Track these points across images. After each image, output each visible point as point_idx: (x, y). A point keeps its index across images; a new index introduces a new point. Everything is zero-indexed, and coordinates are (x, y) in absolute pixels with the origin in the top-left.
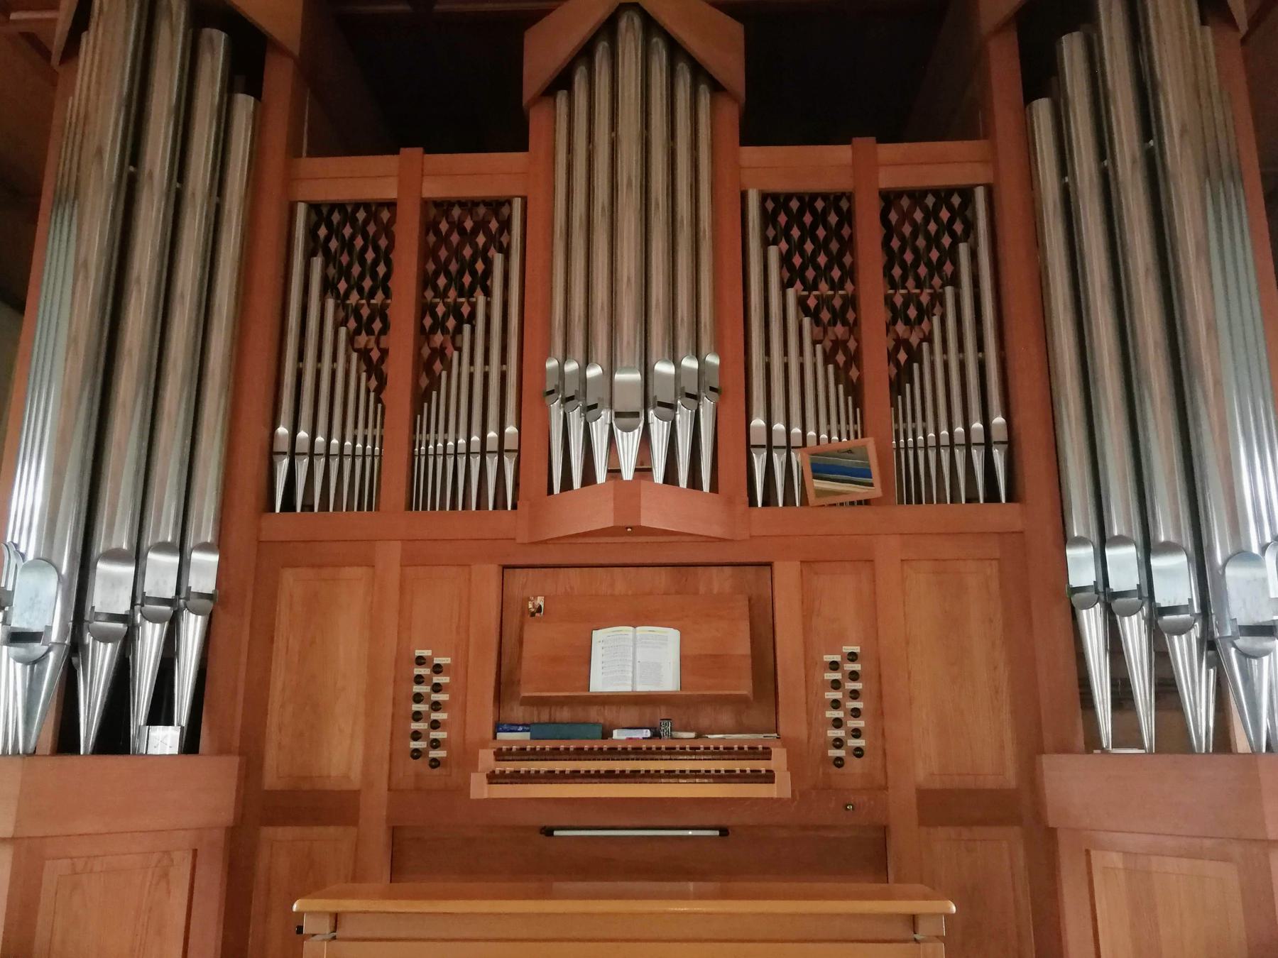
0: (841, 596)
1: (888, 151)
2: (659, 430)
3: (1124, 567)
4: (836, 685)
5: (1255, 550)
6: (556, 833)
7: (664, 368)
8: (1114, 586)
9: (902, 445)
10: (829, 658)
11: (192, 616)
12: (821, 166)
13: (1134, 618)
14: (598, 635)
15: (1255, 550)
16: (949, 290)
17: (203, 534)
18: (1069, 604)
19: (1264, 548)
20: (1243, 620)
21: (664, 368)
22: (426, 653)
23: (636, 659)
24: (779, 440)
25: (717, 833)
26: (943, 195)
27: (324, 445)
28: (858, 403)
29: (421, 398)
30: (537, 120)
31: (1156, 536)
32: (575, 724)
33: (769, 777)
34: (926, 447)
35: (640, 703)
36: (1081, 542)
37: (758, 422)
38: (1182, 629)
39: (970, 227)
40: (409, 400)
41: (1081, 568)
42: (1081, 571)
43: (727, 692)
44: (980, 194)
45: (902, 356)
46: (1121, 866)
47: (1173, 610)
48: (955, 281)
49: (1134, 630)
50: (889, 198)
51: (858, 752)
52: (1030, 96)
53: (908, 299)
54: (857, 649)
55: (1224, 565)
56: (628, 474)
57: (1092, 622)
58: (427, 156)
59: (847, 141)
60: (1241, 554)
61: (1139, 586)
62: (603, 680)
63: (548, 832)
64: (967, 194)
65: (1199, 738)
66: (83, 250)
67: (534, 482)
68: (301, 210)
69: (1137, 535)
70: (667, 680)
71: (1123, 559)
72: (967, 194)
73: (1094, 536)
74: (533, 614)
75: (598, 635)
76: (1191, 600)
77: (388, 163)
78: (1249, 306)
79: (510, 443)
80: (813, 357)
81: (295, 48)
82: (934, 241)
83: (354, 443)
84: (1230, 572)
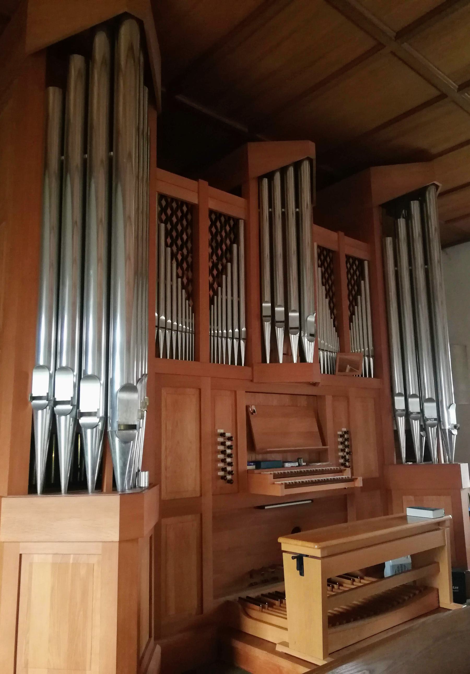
1: (348, 240)
3: (65, 387)
6: (266, 508)
9: (212, 334)
12: (186, 189)
16: (229, 264)
25: (310, 501)
34: (214, 336)
43: (312, 448)
46: (413, 500)
47: (89, 414)
48: (231, 261)
52: (385, 234)
57: (401, 421)
58: (158, 169)
59: (196, 179)
63: (262, 507)
64: (236, 221)
65: (434, 459)
66: (127, 209)
74: (252, 414)
83: (214, 331)
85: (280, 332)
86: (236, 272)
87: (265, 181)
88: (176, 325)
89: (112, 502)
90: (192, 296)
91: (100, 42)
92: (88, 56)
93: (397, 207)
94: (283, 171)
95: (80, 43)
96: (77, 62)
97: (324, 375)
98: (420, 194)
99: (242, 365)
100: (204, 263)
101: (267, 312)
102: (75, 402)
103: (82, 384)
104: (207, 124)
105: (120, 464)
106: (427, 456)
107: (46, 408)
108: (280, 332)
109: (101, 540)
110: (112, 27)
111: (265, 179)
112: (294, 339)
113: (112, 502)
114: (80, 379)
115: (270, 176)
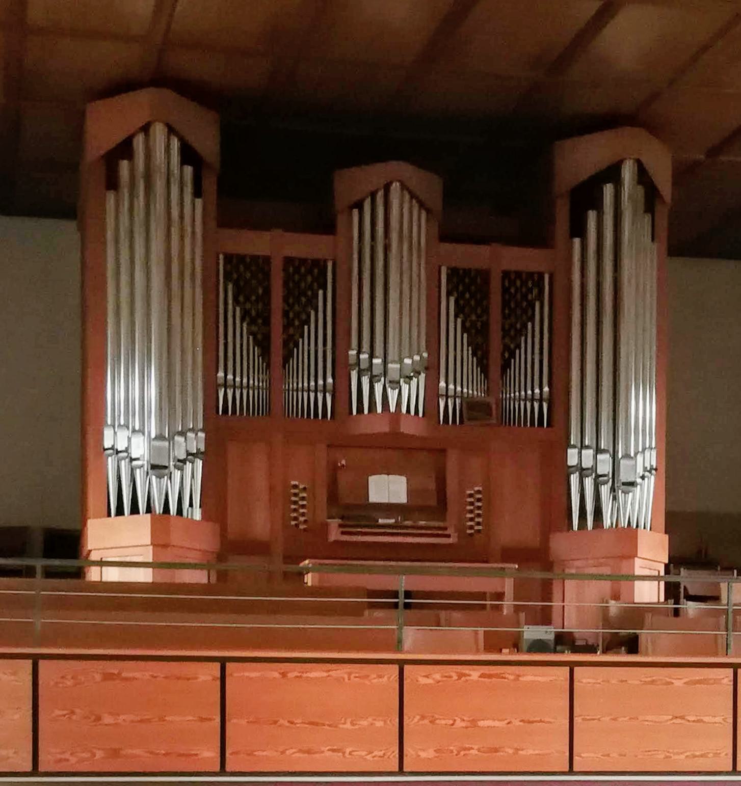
0: (476, 464)
2: (405, 388)
4: (472, 504)
5: (632, 455)
7: (408, 361)
8: (584, 466)
10: (469, 492)
11: (199, 460)
13: (590, 478)
15: (632, 455)
17: (199, 425)
18: (567, 471)
19: (636, 454)
20: (624, 480)
22: (296, 483)
23: (388, 488)
24: (451, 393)
27: (239, 382)
28: (486, 377)
29: (286, 360)
31: (330, 537)
33: (449, 536)
35: (389, 509)
36: (574, 447)
37: (442, 384)
38: (606, 483)
39: (541, 292)
41: (572, 457)
42: (572, 460)
44: (547, 277)
45: (507, 355)
48: (532, 319)
49: (589, 482)
51: (479, 531)
54: (481, 489)
55: (621, 458)
56: (392, 409)
57: (574, 479)
60: (627, 456)
61: (592, 466)
62: (374, 498)
67: (342, 409)
68: (221, 256)
69: (594, 446)
71: (588, 454)
72: (541, 276)
73: (579, 445)
76: (609, 473)
77: (267, 236)
78: (651, 349)
80: (468, 352)
81: (217, 165)
82: (525, 297)
84: (622, 461)
85: (365, 381)
87: (356, 212)
88: (243, 381)
90: (265, 352)
92: (618, 182)
94: (373, 195)
96: (608, 190)
97: (533, 428)
98: (612, 173)
99: (544, 426)
102: (594, 469)
103: (598, 456)
104: (275, 162)
105: (114, 504)
106: (180, 512)
107: (125, 460)
108: (365, 381)
111: (354, 210)
112: (378, 388)
114: (597, 451)
115: (359, 205)
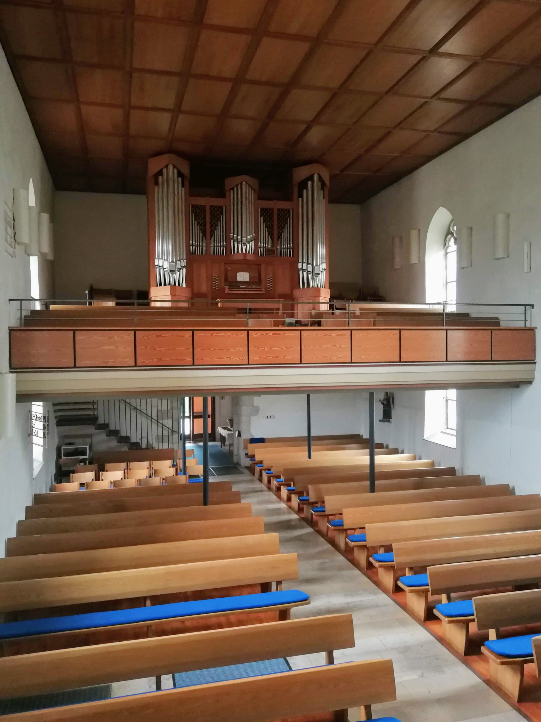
7: (249, 237)
14: (238, 274)
18: (298, 270)
21: (249, 237)
23: (243, 276)
26: (286, 210)
28: (273, 241)
30: (227, 193)
32: (235, 284)
40: (512, 378)
42: (300, 267)
49: (305, 274)
50: (278, 210)
52: (299, 197)
53: (281, 226)
56: (244, 252)
57: (301, 273)
60: (317, 265)
62: (239, 279)
70: (248, 280)
71: (305, 265)
72: (289, 210)
75: (238, 274)
77: (204, 199)
79: (225, 245)
80: (267, 234)
85: (236, 243)
86: (221, 226)
87: (232, 191)
88: (198, 244)
89: (168, 287)
91: (165, 171)
93: (303, 185)
94: (237, 186)
95: (160, 173)
98: (311, 178)
100: (208, 225)
101: (231, 237)
108: (236, 243)
109: (444, 261)
110: (167, 166)
112: (240, 245)
113: (168, 287)
115: (233, 189)
